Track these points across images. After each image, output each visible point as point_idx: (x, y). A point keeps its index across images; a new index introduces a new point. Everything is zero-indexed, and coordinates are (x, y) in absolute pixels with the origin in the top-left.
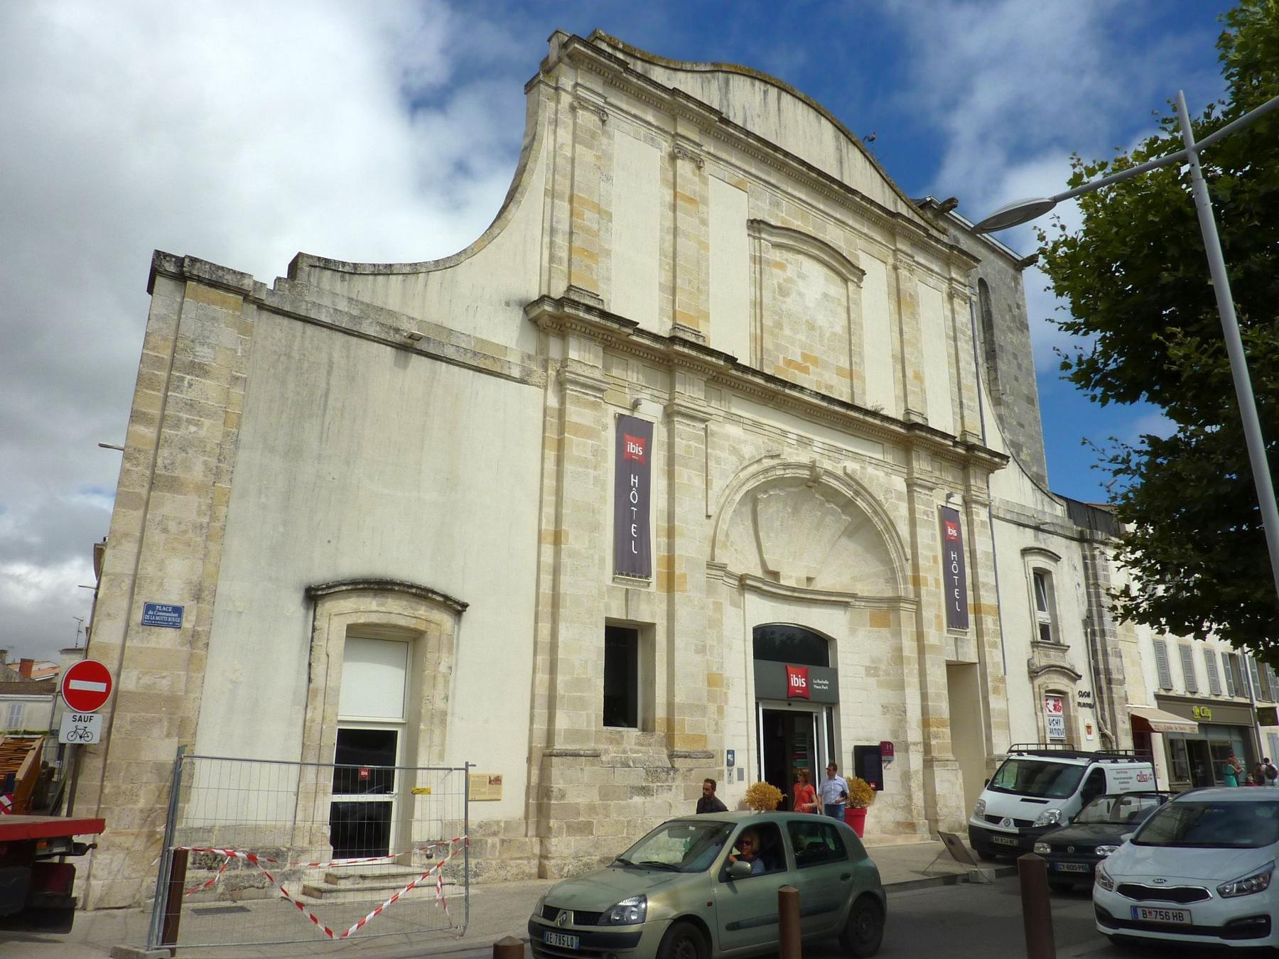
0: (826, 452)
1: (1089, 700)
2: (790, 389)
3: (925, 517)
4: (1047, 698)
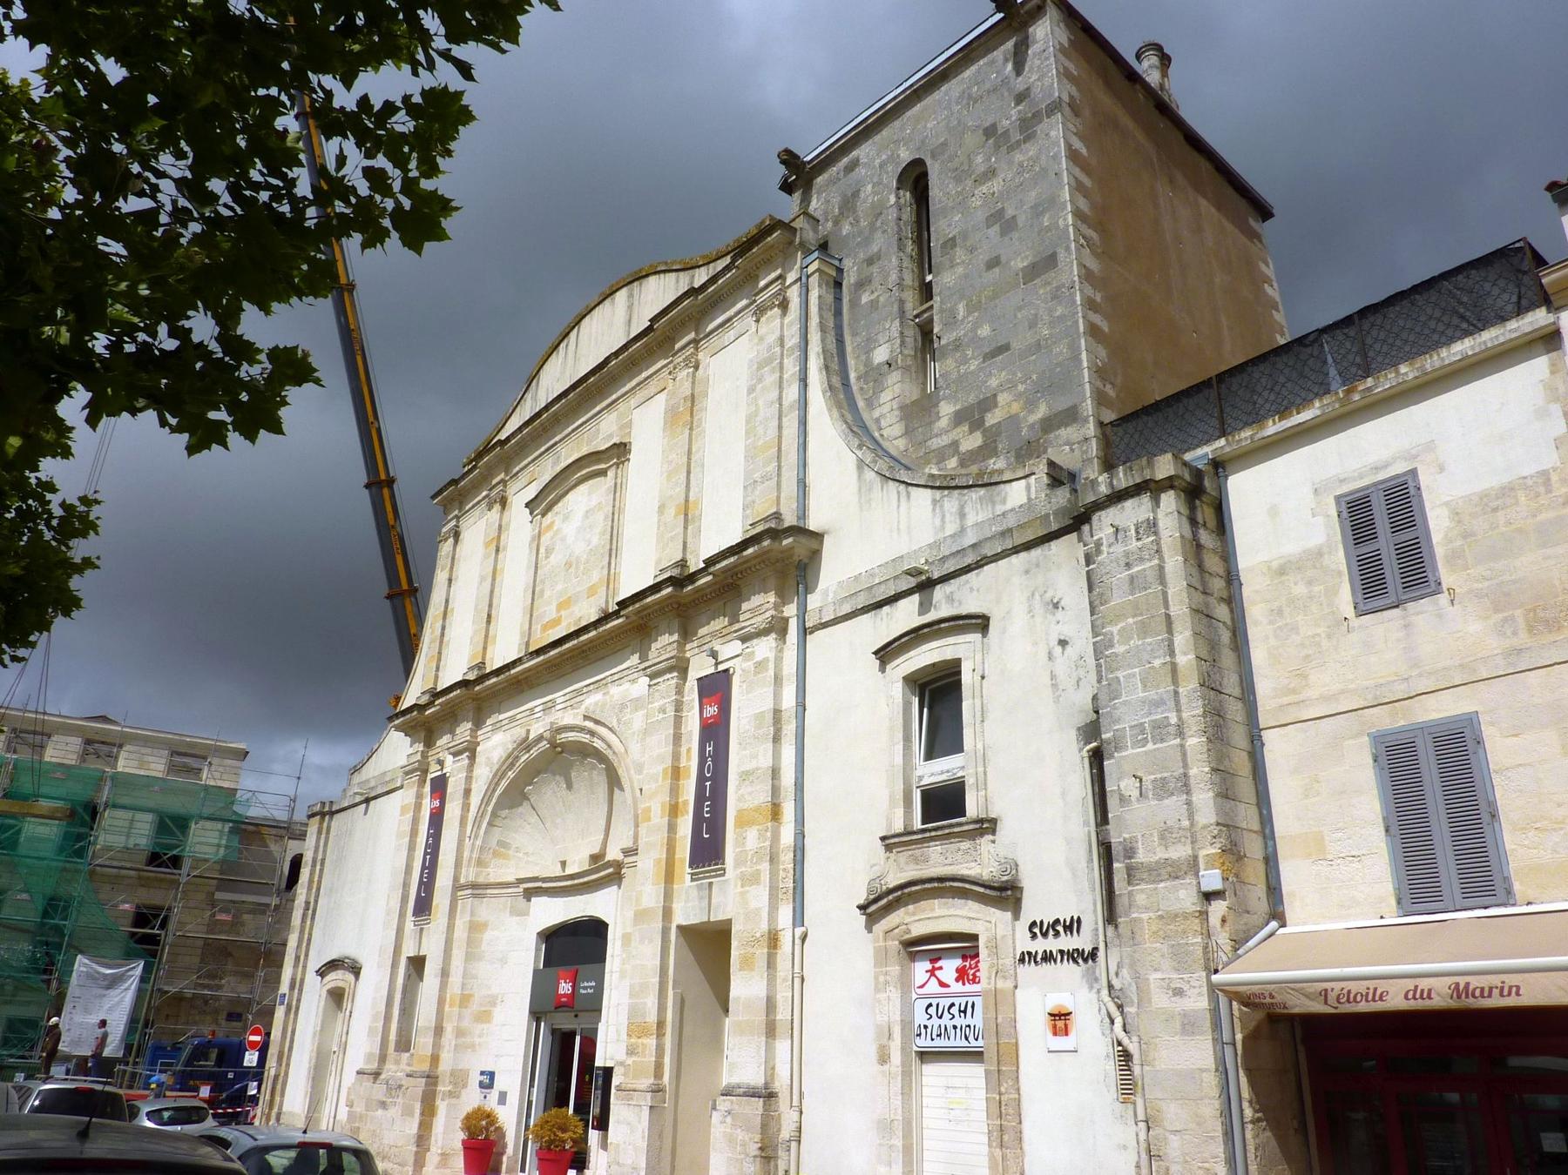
0: (568, 703)
1: (1081, 942)
2: (514, 668)
3: (661, 716)
4: (913, 957)
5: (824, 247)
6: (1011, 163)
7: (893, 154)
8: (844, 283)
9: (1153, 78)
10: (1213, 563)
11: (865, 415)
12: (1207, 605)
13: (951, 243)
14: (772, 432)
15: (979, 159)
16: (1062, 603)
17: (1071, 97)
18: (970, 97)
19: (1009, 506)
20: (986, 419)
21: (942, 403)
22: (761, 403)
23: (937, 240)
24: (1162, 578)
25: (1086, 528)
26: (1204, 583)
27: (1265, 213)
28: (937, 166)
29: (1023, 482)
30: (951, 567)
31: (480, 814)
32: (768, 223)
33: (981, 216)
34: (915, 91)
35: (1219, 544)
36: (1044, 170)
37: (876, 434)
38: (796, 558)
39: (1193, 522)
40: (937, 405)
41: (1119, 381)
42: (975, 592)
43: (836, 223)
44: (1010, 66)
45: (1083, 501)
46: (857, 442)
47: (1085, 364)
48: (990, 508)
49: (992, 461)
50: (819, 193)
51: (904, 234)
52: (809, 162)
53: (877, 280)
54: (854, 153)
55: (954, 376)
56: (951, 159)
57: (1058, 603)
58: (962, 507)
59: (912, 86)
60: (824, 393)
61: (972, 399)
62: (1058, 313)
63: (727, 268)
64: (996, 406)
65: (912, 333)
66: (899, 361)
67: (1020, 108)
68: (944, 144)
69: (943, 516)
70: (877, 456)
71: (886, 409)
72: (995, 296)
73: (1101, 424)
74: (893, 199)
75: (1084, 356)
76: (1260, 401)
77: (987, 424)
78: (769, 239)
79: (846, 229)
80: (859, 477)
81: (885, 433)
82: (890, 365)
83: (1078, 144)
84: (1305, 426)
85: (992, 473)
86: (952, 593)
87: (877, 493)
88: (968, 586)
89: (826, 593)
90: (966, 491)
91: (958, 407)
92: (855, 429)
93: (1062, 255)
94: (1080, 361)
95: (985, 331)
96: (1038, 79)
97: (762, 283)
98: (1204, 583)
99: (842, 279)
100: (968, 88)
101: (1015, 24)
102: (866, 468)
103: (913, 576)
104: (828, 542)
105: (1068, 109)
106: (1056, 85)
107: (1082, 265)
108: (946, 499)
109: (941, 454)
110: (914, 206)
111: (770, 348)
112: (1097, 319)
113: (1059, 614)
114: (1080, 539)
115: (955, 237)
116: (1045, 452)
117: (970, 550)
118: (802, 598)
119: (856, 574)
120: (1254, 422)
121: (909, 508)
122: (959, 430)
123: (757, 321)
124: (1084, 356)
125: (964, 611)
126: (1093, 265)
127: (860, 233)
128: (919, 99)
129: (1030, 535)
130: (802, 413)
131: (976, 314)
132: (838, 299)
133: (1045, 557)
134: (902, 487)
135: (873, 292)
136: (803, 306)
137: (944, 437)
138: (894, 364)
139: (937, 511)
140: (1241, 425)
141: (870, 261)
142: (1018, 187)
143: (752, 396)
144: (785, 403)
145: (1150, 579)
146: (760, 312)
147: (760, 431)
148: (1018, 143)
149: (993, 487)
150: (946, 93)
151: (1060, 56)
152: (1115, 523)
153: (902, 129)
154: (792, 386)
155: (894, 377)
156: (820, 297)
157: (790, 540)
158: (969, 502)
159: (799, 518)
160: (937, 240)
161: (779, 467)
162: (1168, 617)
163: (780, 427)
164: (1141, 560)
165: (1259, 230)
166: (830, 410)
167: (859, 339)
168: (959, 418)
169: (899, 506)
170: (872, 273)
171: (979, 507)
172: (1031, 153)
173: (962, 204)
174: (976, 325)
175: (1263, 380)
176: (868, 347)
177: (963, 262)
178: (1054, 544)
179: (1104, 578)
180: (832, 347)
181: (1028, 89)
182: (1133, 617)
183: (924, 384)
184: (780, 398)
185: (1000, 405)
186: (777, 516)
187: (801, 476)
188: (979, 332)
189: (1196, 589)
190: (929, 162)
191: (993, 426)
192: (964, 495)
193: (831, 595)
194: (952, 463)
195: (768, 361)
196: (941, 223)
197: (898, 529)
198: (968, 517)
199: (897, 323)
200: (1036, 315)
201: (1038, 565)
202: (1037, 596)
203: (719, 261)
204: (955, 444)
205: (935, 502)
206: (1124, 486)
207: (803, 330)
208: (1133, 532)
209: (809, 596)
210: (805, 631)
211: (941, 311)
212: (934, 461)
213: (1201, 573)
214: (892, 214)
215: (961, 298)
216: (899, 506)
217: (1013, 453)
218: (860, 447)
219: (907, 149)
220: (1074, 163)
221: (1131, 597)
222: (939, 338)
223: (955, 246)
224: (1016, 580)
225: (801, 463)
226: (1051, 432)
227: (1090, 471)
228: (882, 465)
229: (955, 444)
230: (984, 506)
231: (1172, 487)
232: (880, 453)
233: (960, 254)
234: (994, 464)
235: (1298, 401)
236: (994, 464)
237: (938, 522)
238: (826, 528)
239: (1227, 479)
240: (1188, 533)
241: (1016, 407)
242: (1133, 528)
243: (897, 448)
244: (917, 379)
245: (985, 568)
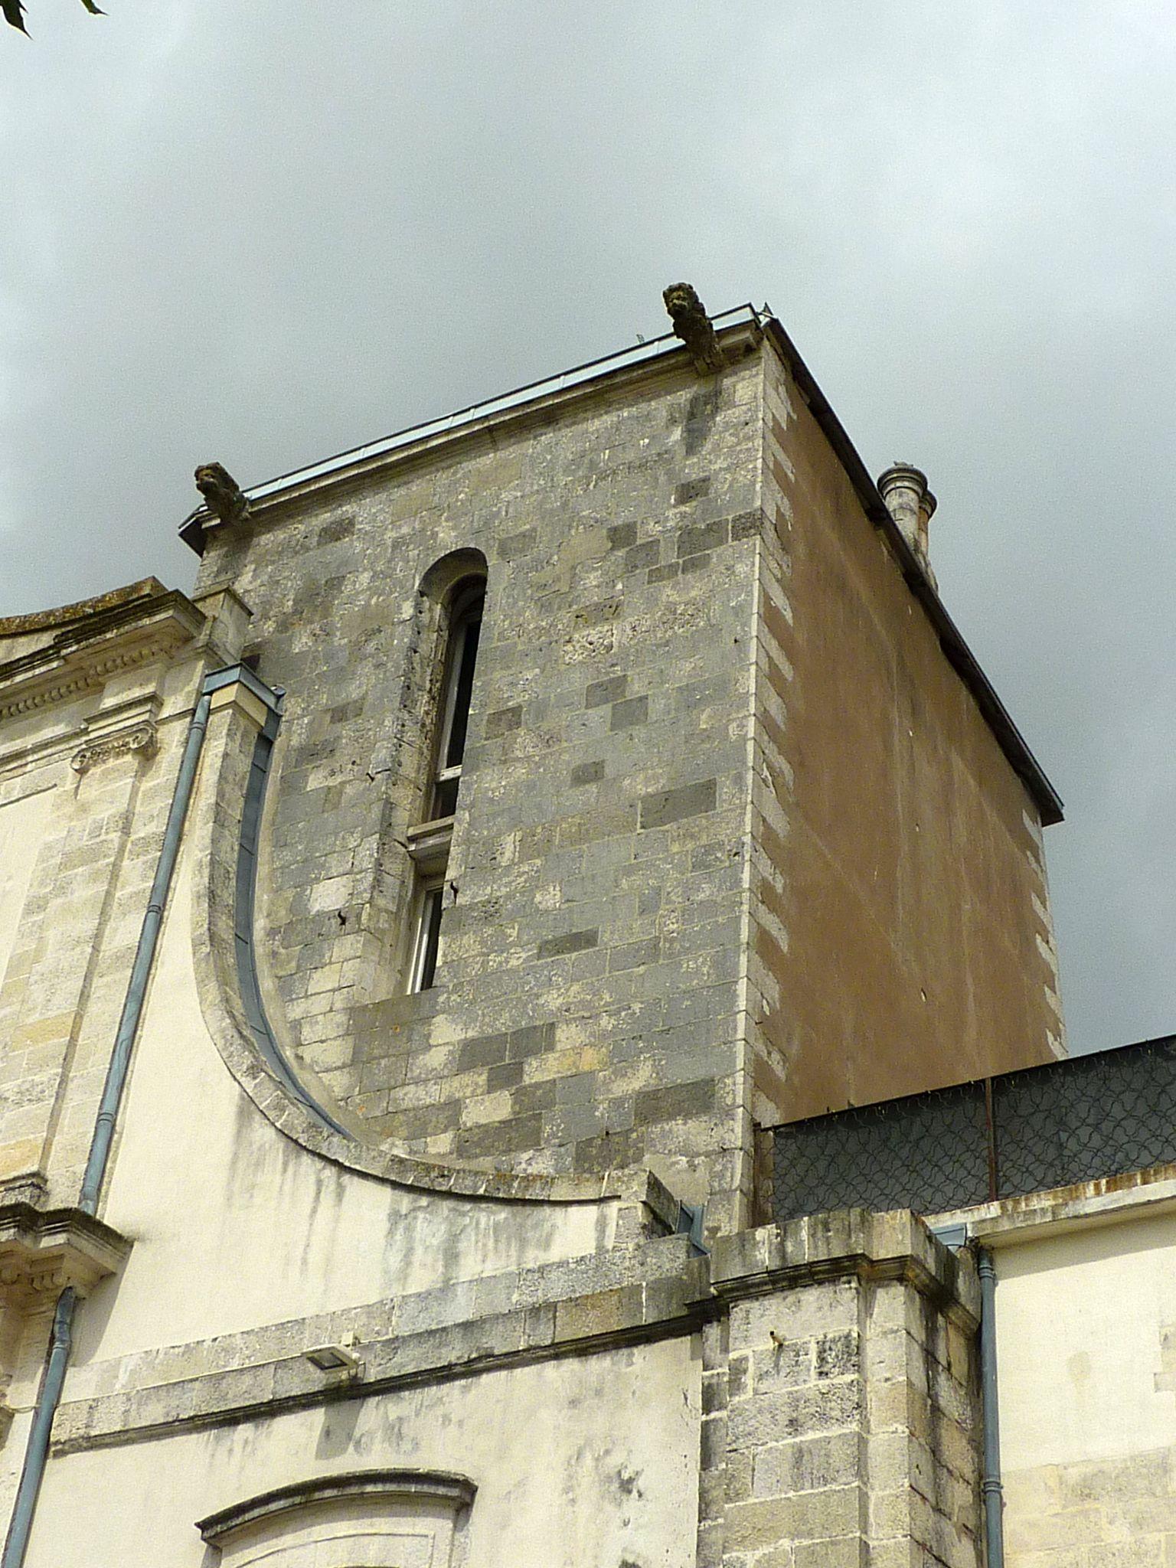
5: (251, 662)
6: (652, 601)
7: (423, 530)
8: (278, 743)
9: (907, 525)
10: (957, 1451)
11: (271, 1010)
12: (940, 1535)
13: (511, 718)
14: (64, 1002)
15: (593, 579)
16: (640, 1483)
17: (779, 514)
18: (593, 466)
19: (555, 1255)
20: (526, 1068)
21: (439, 1019)
22: (52, 935)
23: (484, 705)
24: (860, 1466)
25: (713, 1331)
26: (937, 1488)
27: (1049, 811)
28: (508, 570)
29: (593, 1209)
30: (407, 1362)
31: (277, 1513)
32: (146, 591)
33: (579, 681)
34: (490, 429)
35: (969, 1413)
36: (715, 630)
37: (288, 1053)
38: (61, 1280)
39: (930, 1356)
40: (427, 1020)
41: (794, 1049)
42: (452, 1430)
43: (284, 626)
44: (677, 434)
45: (717, 1274)
46: (248, 1060)
47: (742, 1004)
48: (513, 1252)
49: (525, 1156)
50: (260, 563)
51: (417, 679)
52: (253, 502)
53: (347, 750)
54: (348, 509)
55: (475, 969)
56: (538, 565)
57: (631, 1480)
58: (454, 1238)
59: (486, 417)
60: (196, 944)
61: (504, 1023)
62: (702, 896)
63: (42, 656)
64: (551, 1047)
65: (398, 868)
66: (364, 917)
67: (683, 508)
68: (529, 537)
69: (409, 1251)
70: (286, 1097)
71: (319, 1005)
72: (581, 836)
73: (756, 1128)
74: (407, 610)
75: (742, 987)
76: (1072, 1145)
77: (527, 1080)
78: (146, 621)
79: (302, 642)
80: (239, 1132)
81: (307, 1054)
82: (343, 921)
83: (780, 600)
84: (1158, 1208)
85: (528, 1180)
86: (400, 1419)
87: (271, 1175)
88: (440, 1411)
89: (114, 1367)
90: (468, 1206)
91: (471, 1034)
92: (246, 1032)
93: (725, 789)
94: (734, 996)
95: (550, 898)
96: (727, 469)
97: (109, 702)
98: (937, 1488)
99: (276, 732)
100: (592, 450)
101: (699, 364)
102: (258, 1117)
103: (323, 1368)
104: (138, 1256)
105: (772, 534)
106: (758, 486)
107: (760, 818)
108: (421, 1215)
109: (420, 1124)
110: (445, 634)
111: (97, 830)
112: (772, 923)
113: (632, 1503)
114: (697, 1353)
115: (520, 707)
116: (638, 1159)
117: (458, 1334)
118: (55, 1372)
119: (191, 1340)
120: (1057, 1183)
121: (337, 1220)
122: (466, 1078)
123: (82, 772)
124: (742, 987)
125: (423, 1463)
126: (779, 823)
127: (330, 657)
128: (494, 445)
129: (591, 1326)
130: (139, 978)
131: (538, 862)
132: (260, 770)
133: (618, 1376)
134: (330, 1172)
135: (333, 773)
136: (188, 765)
137: (433, 1089)
138: (352, 919)
139: (398, 1237)
140: (1031, 1183)
141: (339, 714)
142: (658, 646)
143: (36, 918)
144: (108, 948)
145: (837, 1461)
146: (90, 756)
147: (38, 994)
148: (673, 569)
149: (528, 1210)
150: (549, 448)
151: (772, 440)
152: (778, 1333)
153: (452, 488)
154: (129, 918)
155: (349, 945)
156: (226, 755)
157: (61, 1239)
158: (471, 1232)
159: (84, 1196)
160: (484, 705)
161: (64, 1081)
162: (865, 1547)
163: (84, 996)
164: (824, 1418)
165: (1036, 837)
166: (201, 983)
167: (287, 855)
168: (469, 1056)
169: (314, 1211)
170: (339, 738)
171: (491, 1244)
172: (693, 593)
173: (545, 652)
174: (536, 883)
175: (1082, 1108)
176: (307, 873)
177: (529, 757)
178: (640, 1353)
179: (740, 1444)
180: (230, 854)
181: (705, 480)
182: (793, 1536)
183: (404, 973)
184: (98, 936)
185: (559, 1047)
186: (37, 1181)
187: (109, 1107)
188: (538, 898)
189: (924, 1498)
190: (492, 561)
191: (537, 1086)
192: (464, 1214)
193: (123, 1377)
194: (440, 1144)
195: (89, 855)
196: (497, 675)
197: (304, 1261)
198: (462, 1261)
199: (373, 841)
200: (658, 891)
201: (599, 1393)
202: (588, 1460)
203: (23, 640)
204: (454, 1107)
205: (395, 1217)
206: (807, 1258)
207: (177, 811)
208: (813, 1356)
209: (71, 1372)
210: (44, 1449)
211: (468, 841)
212: (404, 1132)
213: (934, 1468)
214: (401, 638)
215: (514, 824)
216: (314, 1211)
217: (571, 1148)
218: (253, 1071)
219: (453, 528)
220: (771, 630)
221: (791, 1494)
222: (456, 891)
223: (518, 724)
224: (549, 1417)
225: (115, 1081)
226: (656, 1121)
227: (723, 1217)
228: (296, 1118)
229: (454, 1107)
230: (502, 1246)
231: (901, 1279)
232: (293, 1093)
233: (524, 742)
234: (529, 1162)
235: (1145, 1158)
236: (529, 1162)
237: (395, 1260)
238: (142, 1228)
239: (995, 1285)
240: (920, 1381)
241: (590, 1060)
242: (813, 1349)
243: (329, 1089)
244: (392, 959)
245: (485, 1378)
